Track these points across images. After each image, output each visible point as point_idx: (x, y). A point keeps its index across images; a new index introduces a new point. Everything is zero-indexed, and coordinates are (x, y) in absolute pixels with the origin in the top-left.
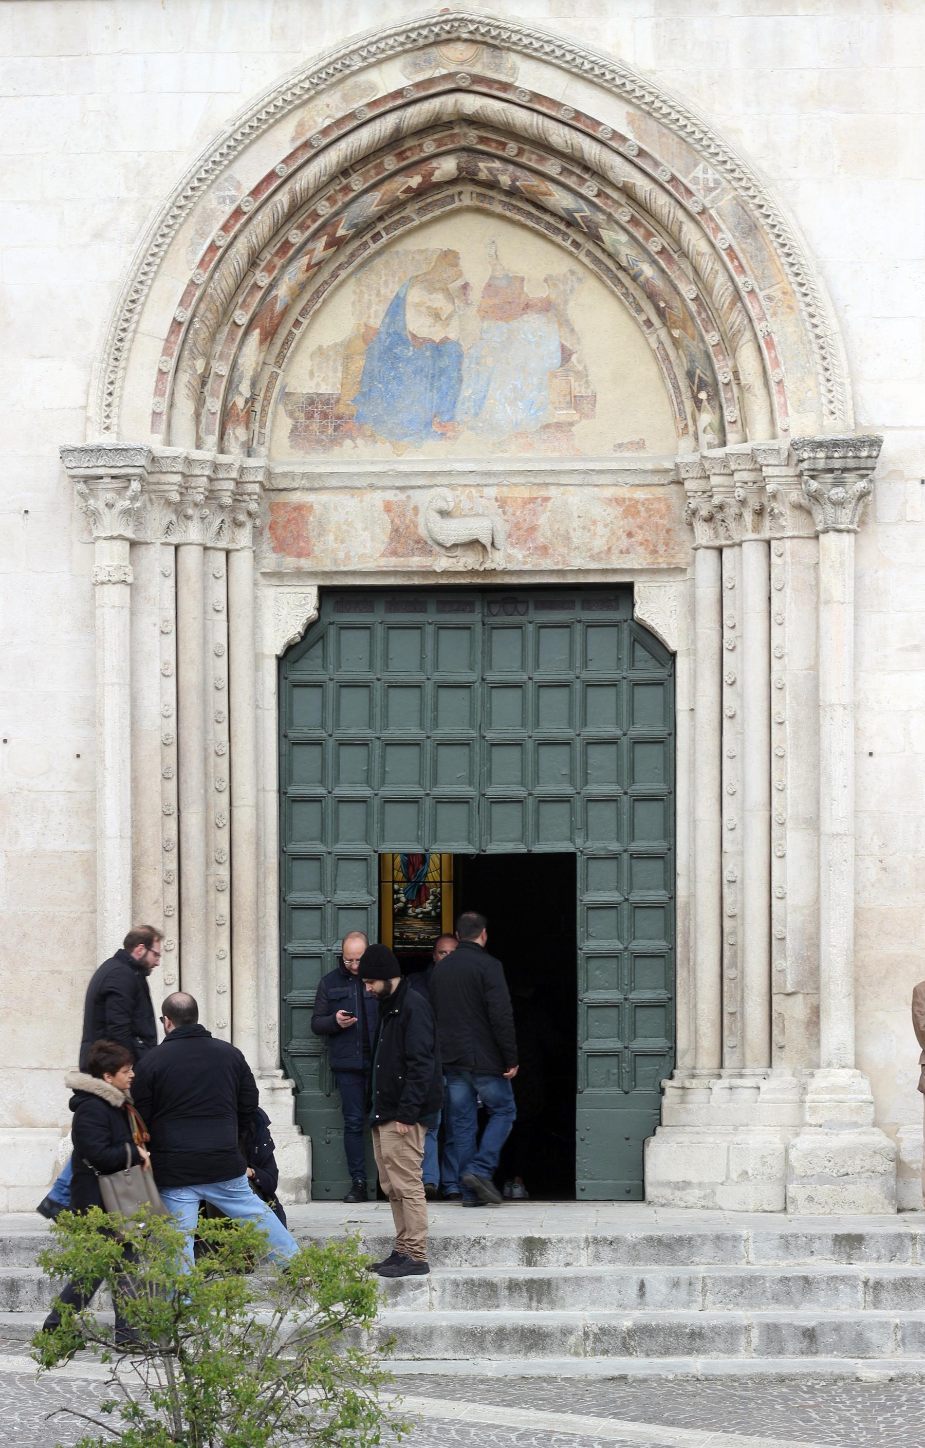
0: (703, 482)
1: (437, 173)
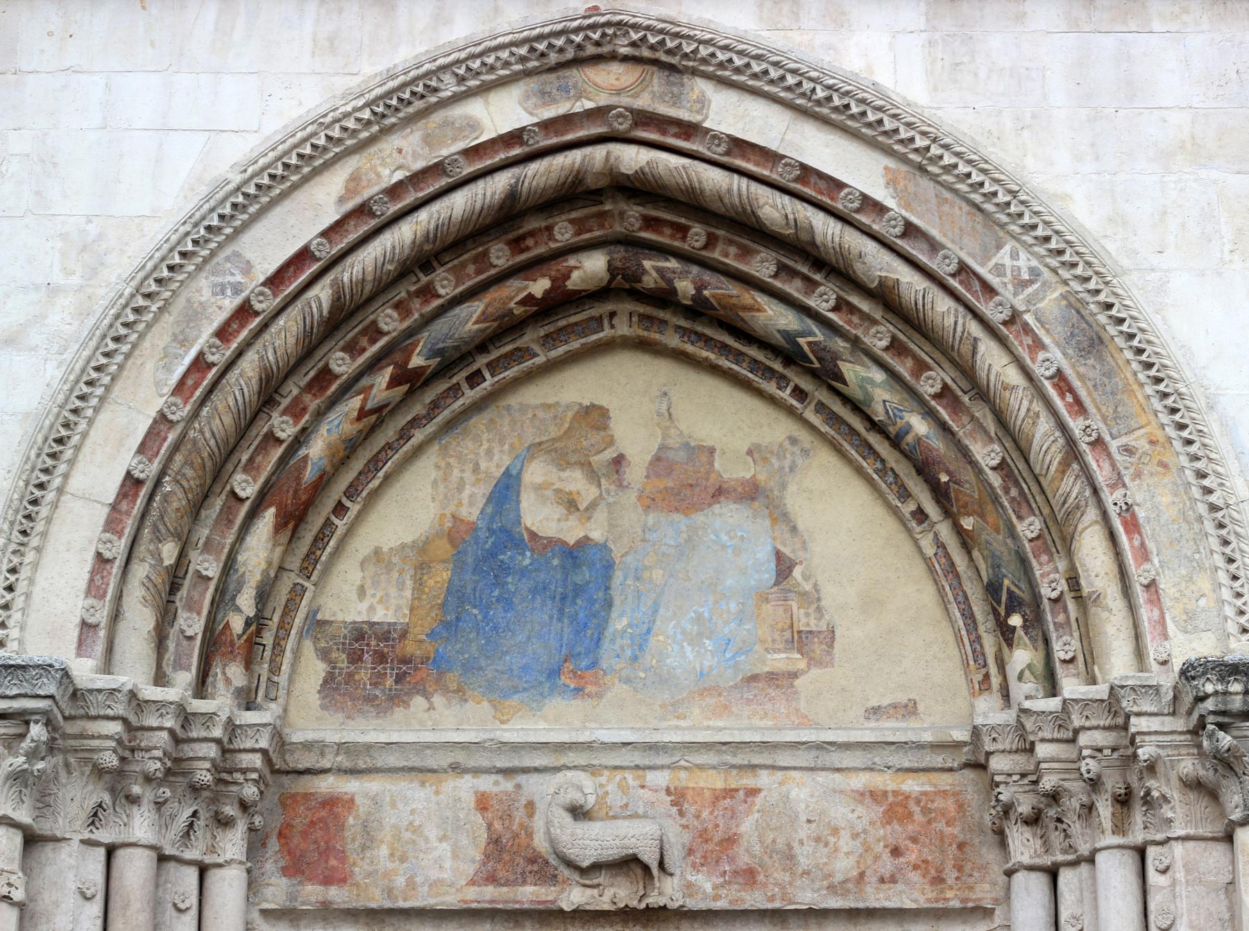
0: (1021, 759)
1: (575, 275)
